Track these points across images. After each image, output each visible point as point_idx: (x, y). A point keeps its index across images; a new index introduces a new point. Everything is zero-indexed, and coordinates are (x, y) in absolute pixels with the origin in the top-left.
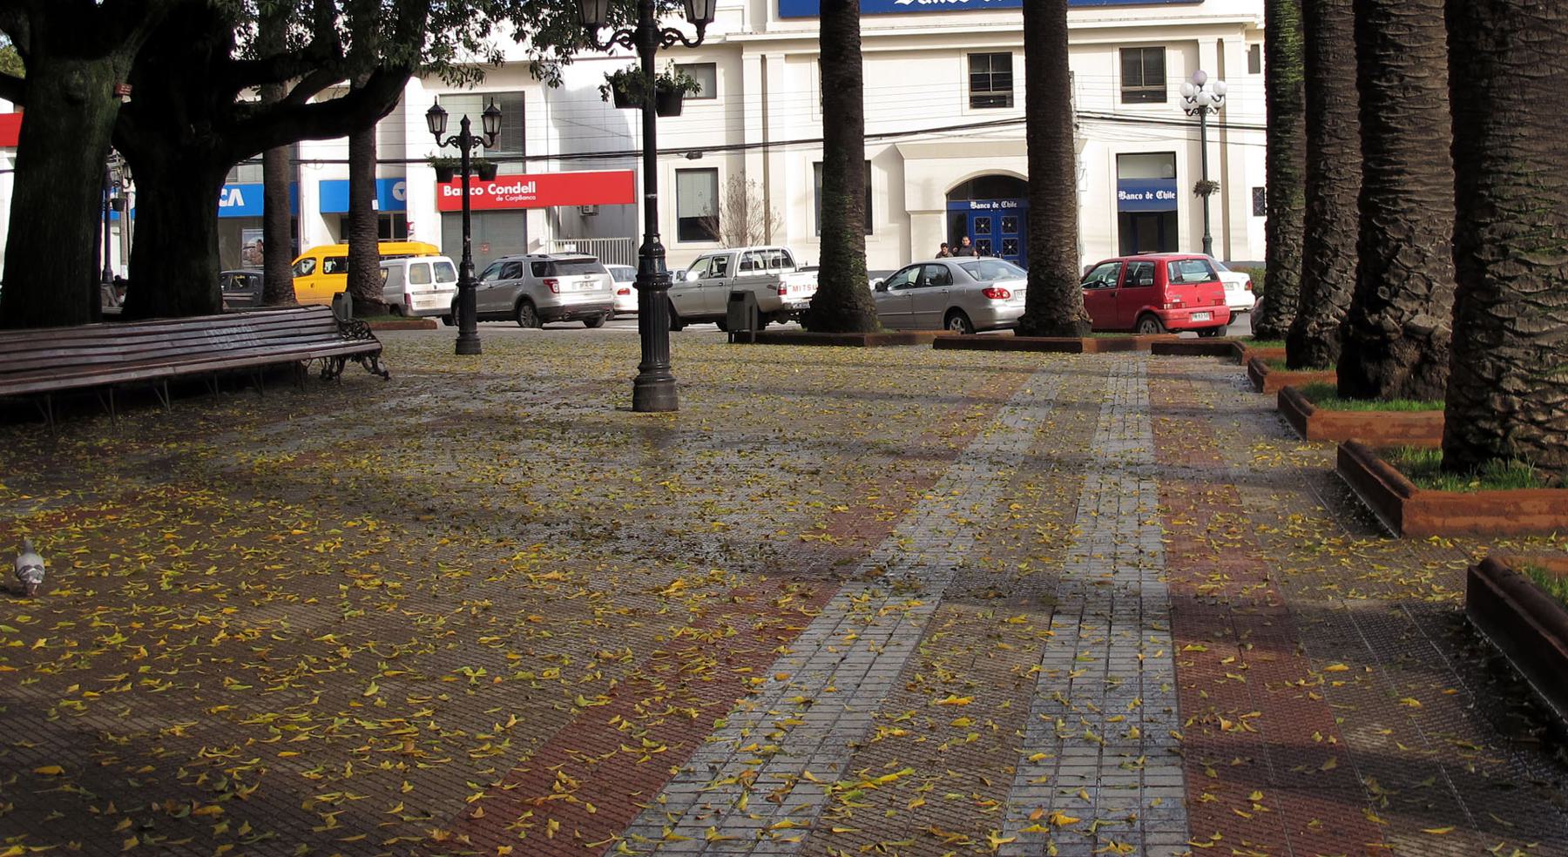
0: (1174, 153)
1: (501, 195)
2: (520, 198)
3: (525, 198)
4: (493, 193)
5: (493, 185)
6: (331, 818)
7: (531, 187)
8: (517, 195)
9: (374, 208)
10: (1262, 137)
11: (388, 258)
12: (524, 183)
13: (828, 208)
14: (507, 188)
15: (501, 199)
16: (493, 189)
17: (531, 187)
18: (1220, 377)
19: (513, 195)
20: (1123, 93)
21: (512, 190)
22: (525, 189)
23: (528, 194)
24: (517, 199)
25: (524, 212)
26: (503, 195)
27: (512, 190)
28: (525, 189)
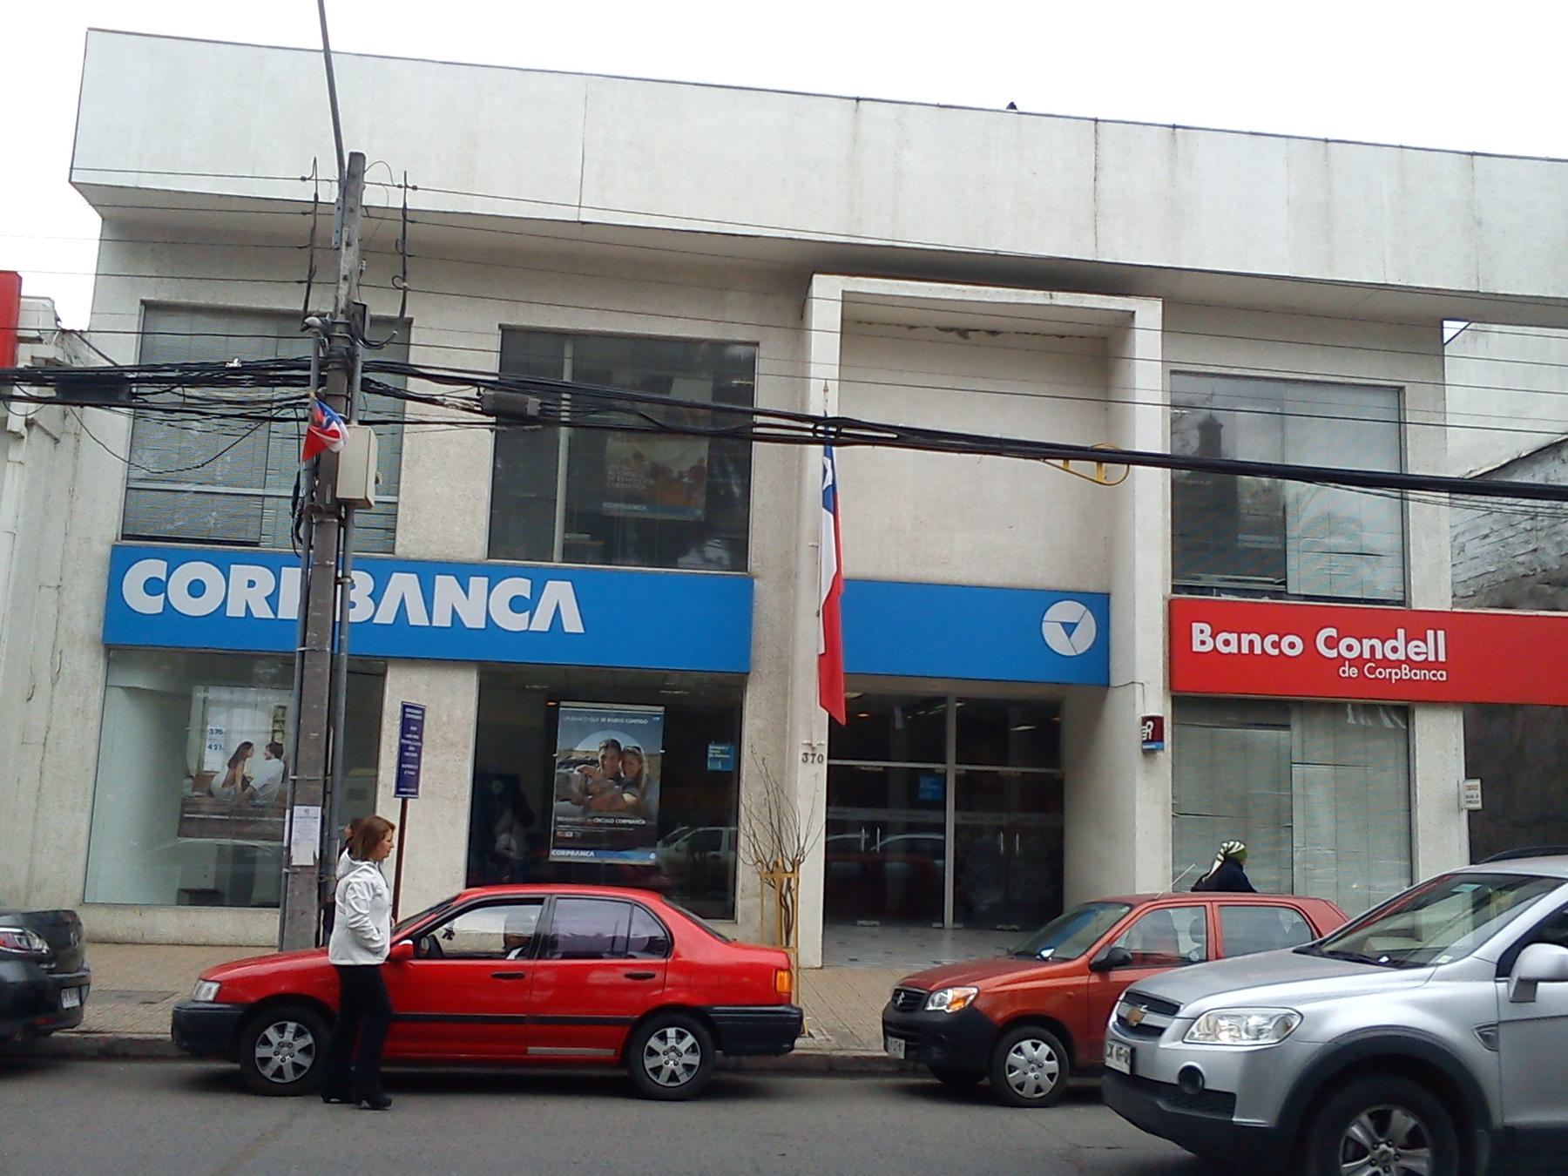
0: (267, 598)
1: (1352, 662)
2: (1405, 672)
3: (1420, 674)
4: (1332, 654)
5: (1333, 632)
6: (435, 536)
7: (1434, 646)
8: (1397, 664)
9: (1443, 632)
10: (839, 335)
11: (403, 748)
12: (1415, 634)
13: (536, 955)
14: (1367, 643)
15: (1354, 672)
16: (1331, 643)
17: (1434, 646)
18: (39, 762)
19: (1386, 663)
20: (1173, 586)
21: (1384, 650)
22: (1417, 650)
23: (1425, 665)
24: (1395, 675)
25: (1405, 713)
26: (1359, 662)
27: (1384, 650)
28: (1417, 650)
